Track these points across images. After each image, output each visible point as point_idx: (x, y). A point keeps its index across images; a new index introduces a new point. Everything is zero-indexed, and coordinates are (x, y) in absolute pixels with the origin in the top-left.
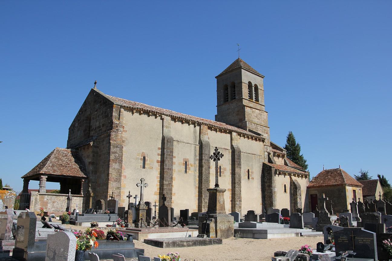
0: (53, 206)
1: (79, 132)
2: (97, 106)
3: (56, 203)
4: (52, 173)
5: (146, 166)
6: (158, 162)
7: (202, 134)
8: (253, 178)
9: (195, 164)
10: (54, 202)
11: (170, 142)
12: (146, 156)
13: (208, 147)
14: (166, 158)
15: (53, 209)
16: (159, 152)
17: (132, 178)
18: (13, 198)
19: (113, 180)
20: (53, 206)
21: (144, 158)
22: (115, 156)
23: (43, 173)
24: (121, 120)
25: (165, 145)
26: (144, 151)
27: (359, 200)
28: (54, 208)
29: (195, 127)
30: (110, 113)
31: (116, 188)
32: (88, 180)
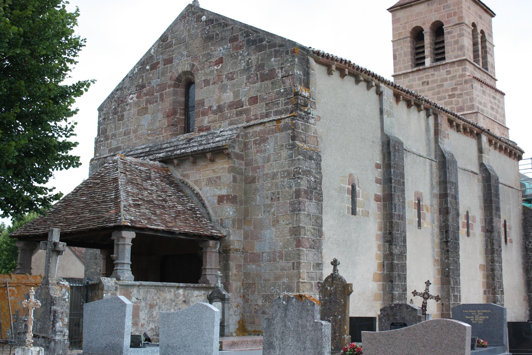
0: (151, 316)
1: (148, 117)
2: (220, 51)
3: (157, 308)
4: (144, 223)
5: (358, 209)
6: (377, 198)
7: (441, 136)
8: (511, 241)
9: (432, 205)
10: (152, 306)
11: (399, 150)
12: (356, 182)
13: (455, 166)
14: (395, 191)
15: (151, 325)
16: (378, 173)
17: (336, 239)
18: (65, 299)
19: (308, 246)
20: (151, 316)
21: (353, 187)
22: (308, 181)
23: (129, 224)
24: (312, 89)
25: (392, 158)
26: (353, 172)
27: (335, 269)
28: (154, 322)
29: (428, 116)
30: (282, 68)
31: (313, 266)
32: (220, 245)
